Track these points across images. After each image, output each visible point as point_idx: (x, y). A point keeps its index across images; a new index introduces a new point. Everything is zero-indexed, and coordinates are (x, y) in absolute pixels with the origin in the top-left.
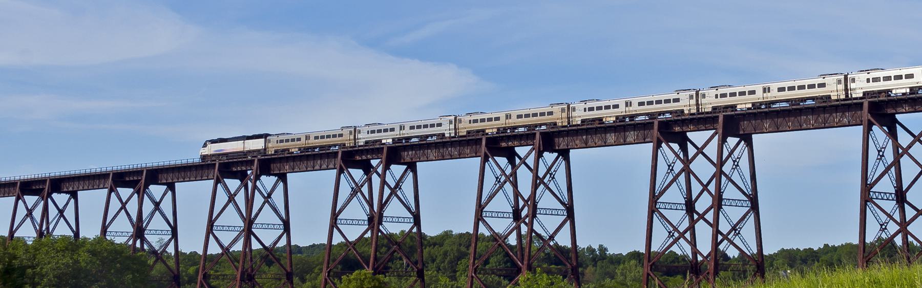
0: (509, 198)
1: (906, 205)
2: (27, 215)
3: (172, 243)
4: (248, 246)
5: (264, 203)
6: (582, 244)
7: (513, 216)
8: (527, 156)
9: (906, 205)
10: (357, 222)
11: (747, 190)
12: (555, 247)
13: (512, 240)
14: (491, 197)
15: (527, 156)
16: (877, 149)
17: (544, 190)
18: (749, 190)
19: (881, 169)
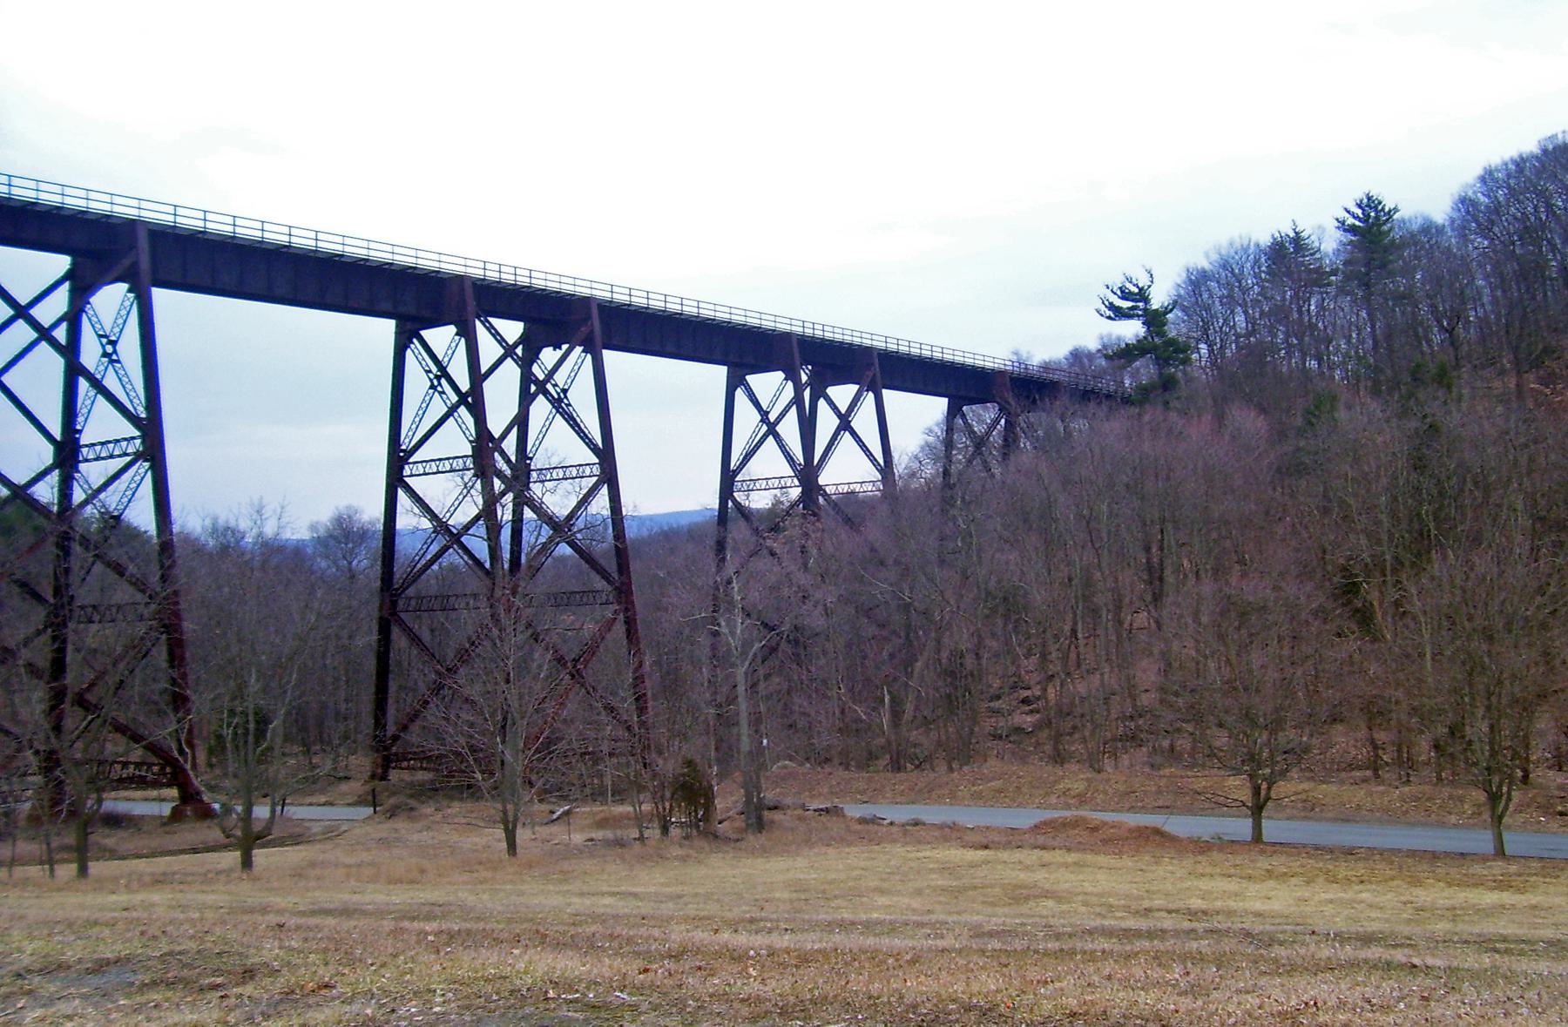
0: (463, 422)
1: (58, 435)
2: (768, 413)
3: (54, 477)
4: (506, 535)
5: (765, 436)
6: (190, 517)
7: (474, 464)
8: (500, 340)
9: (58, 435)
10: (454, 465)
11: (131, 401)
12: (603, 546)
13: (46, 492)
14: (748, 457)
15: (500, 340)
16: (96, 332)
17: (551, 417)
18: (136, 401)
19: (438, 408)
